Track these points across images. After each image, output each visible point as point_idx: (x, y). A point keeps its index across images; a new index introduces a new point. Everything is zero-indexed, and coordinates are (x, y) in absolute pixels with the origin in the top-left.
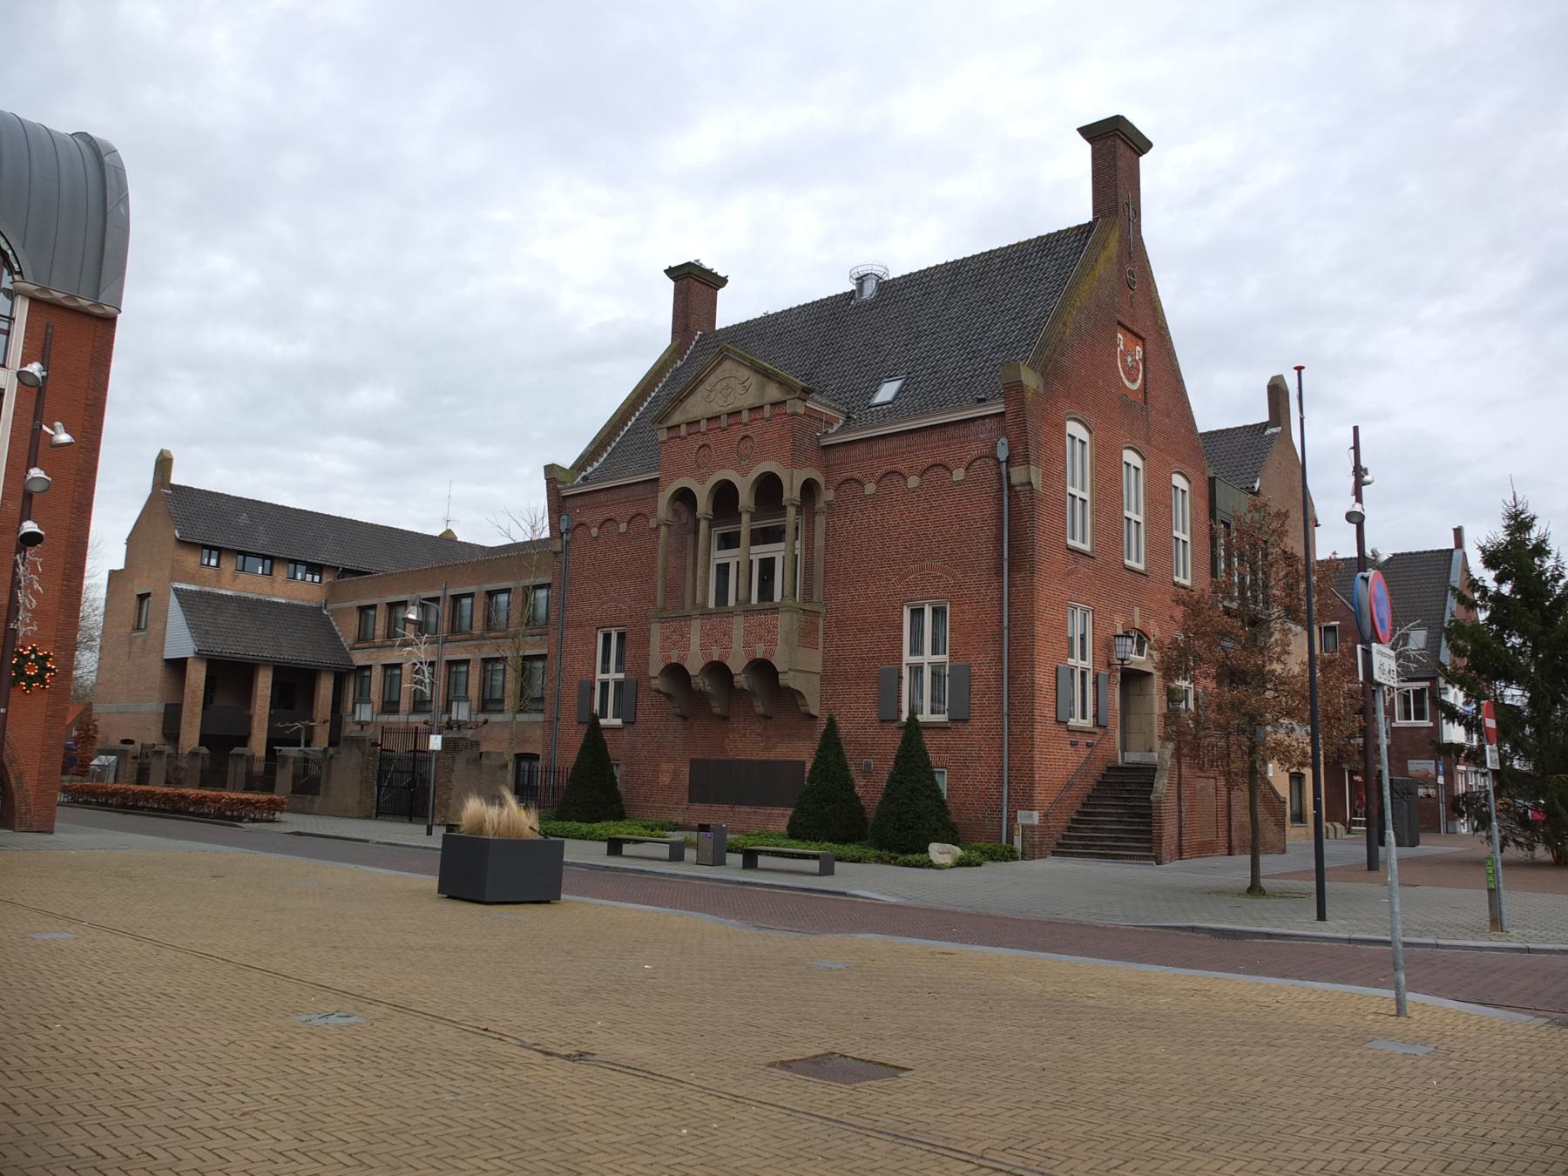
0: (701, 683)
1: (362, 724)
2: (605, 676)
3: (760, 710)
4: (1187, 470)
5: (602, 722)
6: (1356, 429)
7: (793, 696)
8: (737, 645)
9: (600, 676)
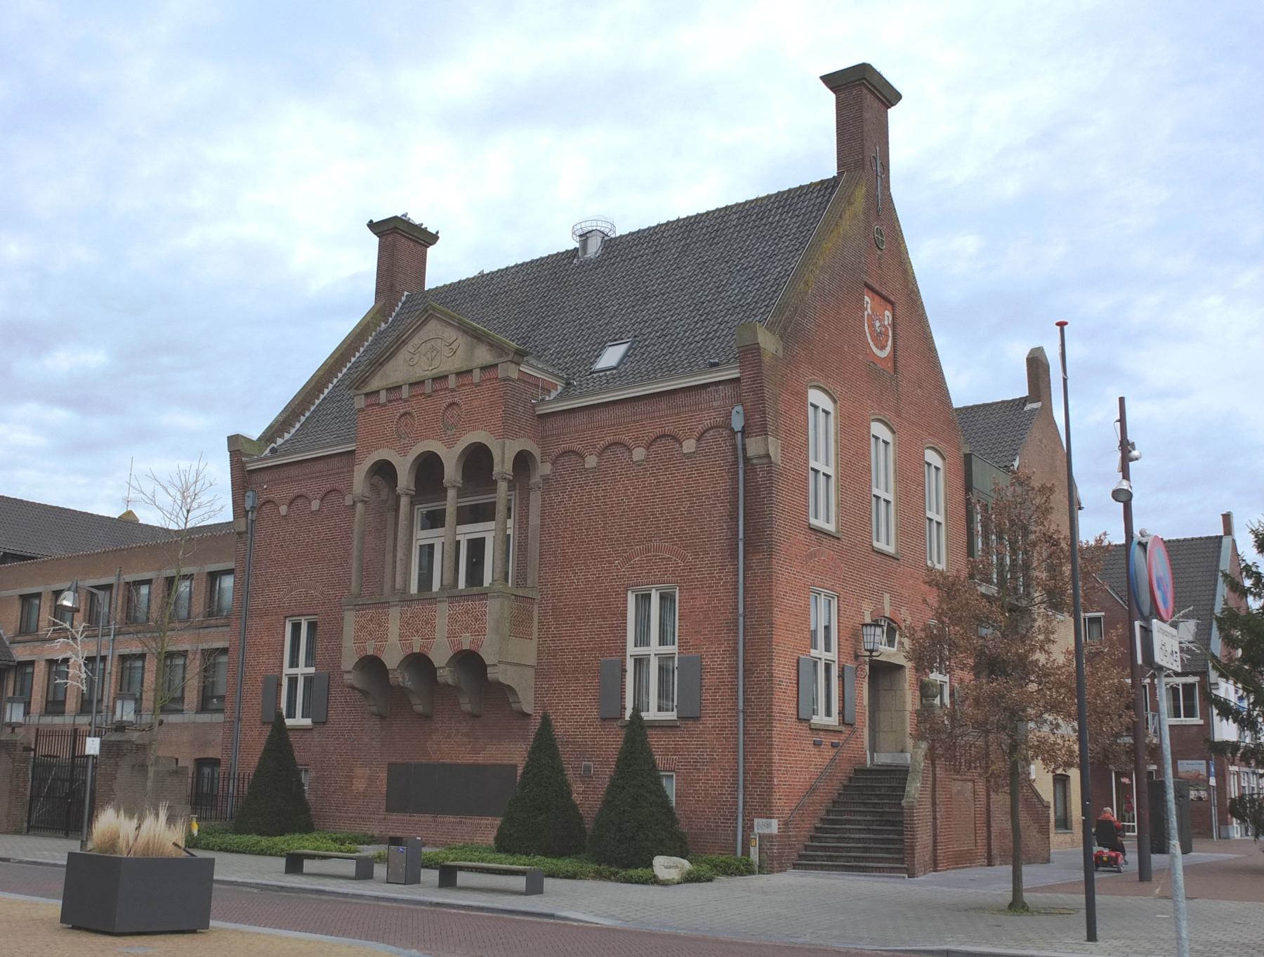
0: (401, 678)
1: (13, 726)
2: (293, 671)
3: (466, 706)
4: (942, 446)
5: (289, 722)
6: (1122, 400)
7: (503, 692)
8: (441, 635)
9: (287, 670)
